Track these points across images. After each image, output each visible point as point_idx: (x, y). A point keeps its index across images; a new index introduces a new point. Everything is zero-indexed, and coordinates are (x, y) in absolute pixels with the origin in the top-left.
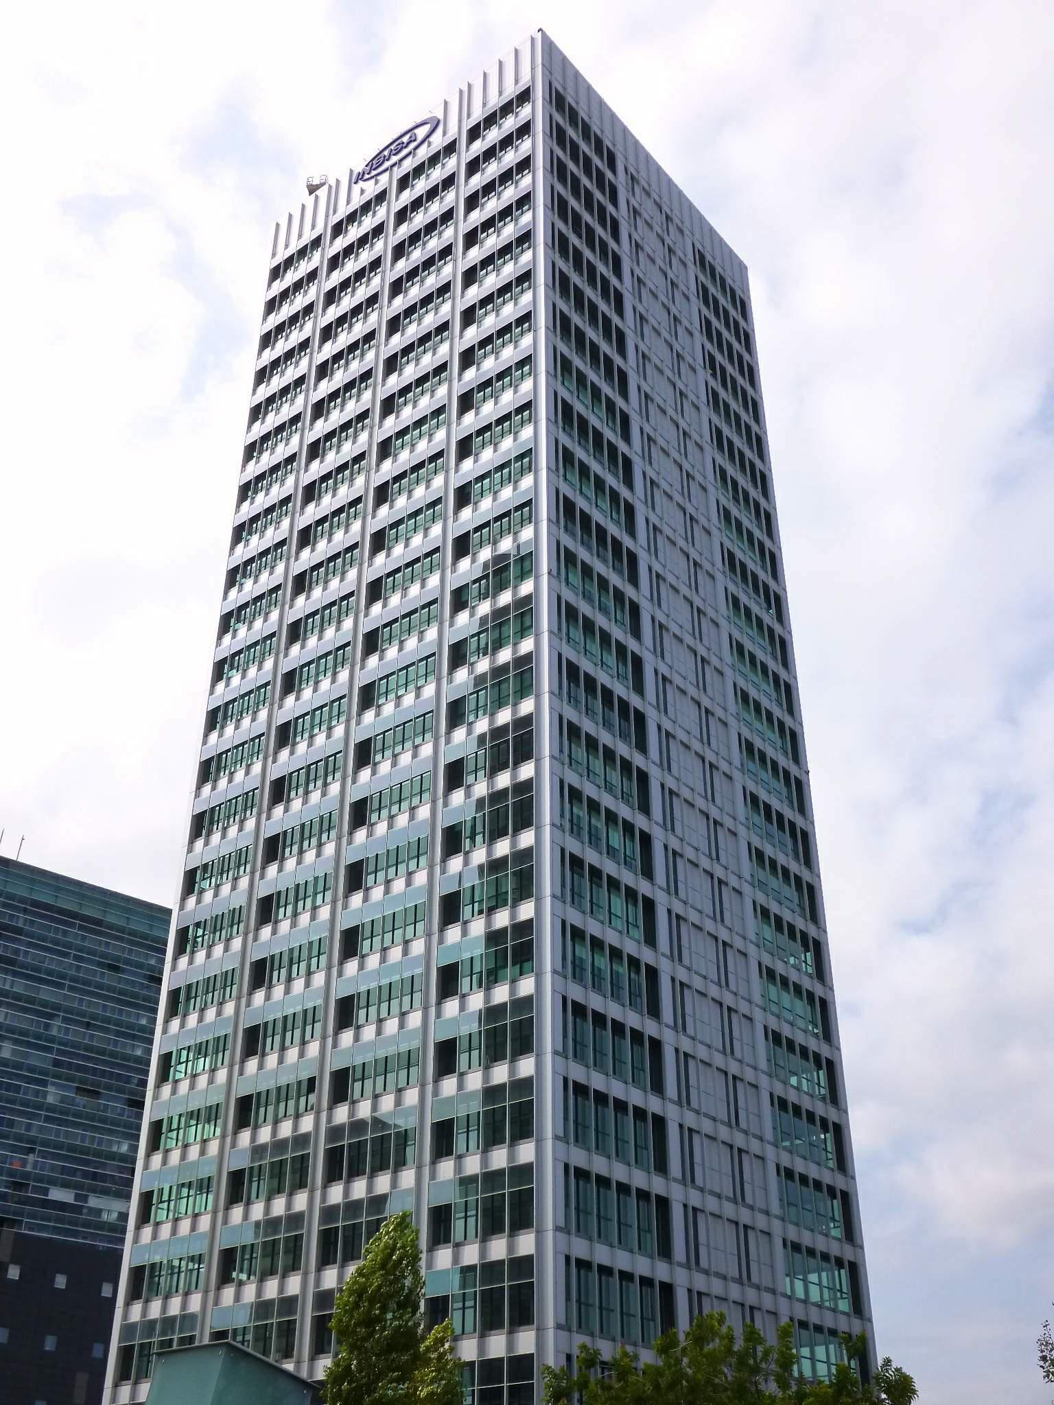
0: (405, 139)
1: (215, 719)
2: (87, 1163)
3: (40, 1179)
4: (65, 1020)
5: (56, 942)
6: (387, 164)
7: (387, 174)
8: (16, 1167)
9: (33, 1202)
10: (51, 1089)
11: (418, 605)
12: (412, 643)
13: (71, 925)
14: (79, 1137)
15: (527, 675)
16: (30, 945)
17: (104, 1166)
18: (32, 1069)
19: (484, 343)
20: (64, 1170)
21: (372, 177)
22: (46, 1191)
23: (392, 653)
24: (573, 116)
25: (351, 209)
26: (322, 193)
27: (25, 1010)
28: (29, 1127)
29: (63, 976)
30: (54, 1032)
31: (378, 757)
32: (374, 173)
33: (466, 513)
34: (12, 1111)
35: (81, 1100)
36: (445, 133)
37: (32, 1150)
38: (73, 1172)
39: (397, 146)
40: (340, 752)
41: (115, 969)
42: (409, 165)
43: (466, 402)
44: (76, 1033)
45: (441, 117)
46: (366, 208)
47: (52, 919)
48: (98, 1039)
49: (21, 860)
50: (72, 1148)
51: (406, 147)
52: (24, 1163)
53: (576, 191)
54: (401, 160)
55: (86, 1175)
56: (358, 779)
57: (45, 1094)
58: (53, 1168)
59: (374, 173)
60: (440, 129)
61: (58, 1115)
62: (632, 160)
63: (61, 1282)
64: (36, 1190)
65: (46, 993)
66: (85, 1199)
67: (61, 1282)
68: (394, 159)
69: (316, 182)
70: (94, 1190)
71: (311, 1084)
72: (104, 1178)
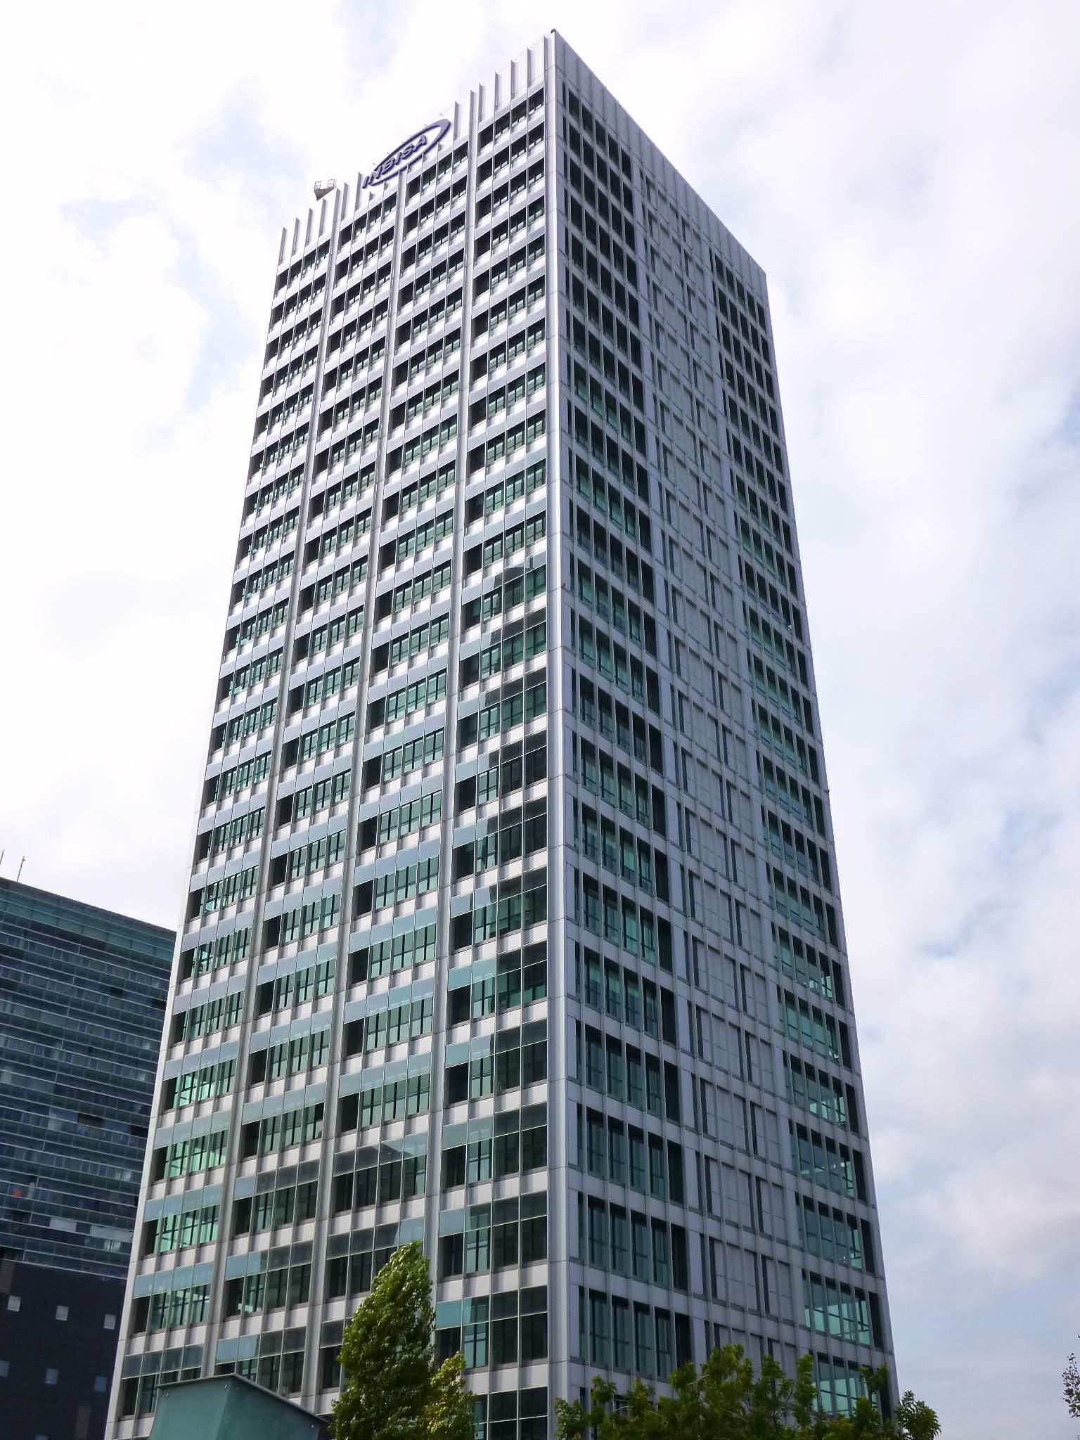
0: (415, 143)
1: (220, 737)
2: (89, 1192)
3: (40, 1208)
4: (67, 1045)
5: (58, 966)
6: (397, 168)
8: (17, 1196)
9: (34, 1232)
10: (52, 1116)
11: (428, 620)
13: (73, 948)
14: (81, 1165)
16: (31, 968)
17: (106, 1195)
18: (33, 1096)
19: (496, 352)
20: (65, 1199)
22: (47, 1221)
23: (402, 669)
24: (587, 119)
25: (359, 214)
26: (330, 198)
27: (26, 1035)
28: (29, 1155)
29: (65, 1001)
30: (56, 1058)
32: (383, 177)
33: (478, 526)
34: (12, 1139)
35: (83, 1127)
36: (455, 137)
37: (32, 1179)
38: (75, 1201)
39: (406, 149)
41: (118, 993)
42: (419, 169)
44: (78, 1059)
45: (452, 120)
46: (375, 213)
47: (54, 942)
48: (101, 1065)
50: (74, 1177)
51: (416, 151)
52: (24, 1192)
53: (590, 195)
54: (411, 164)
55: (88, 1204)
57: (46, 1121)
58: (54, 1197)
61: (60, 1143)
65: (47, 1018)
66: (87, 1229)
68: (404, 163)
69: (324, 186)
70: (96, 1220)
72: (106, 1207)
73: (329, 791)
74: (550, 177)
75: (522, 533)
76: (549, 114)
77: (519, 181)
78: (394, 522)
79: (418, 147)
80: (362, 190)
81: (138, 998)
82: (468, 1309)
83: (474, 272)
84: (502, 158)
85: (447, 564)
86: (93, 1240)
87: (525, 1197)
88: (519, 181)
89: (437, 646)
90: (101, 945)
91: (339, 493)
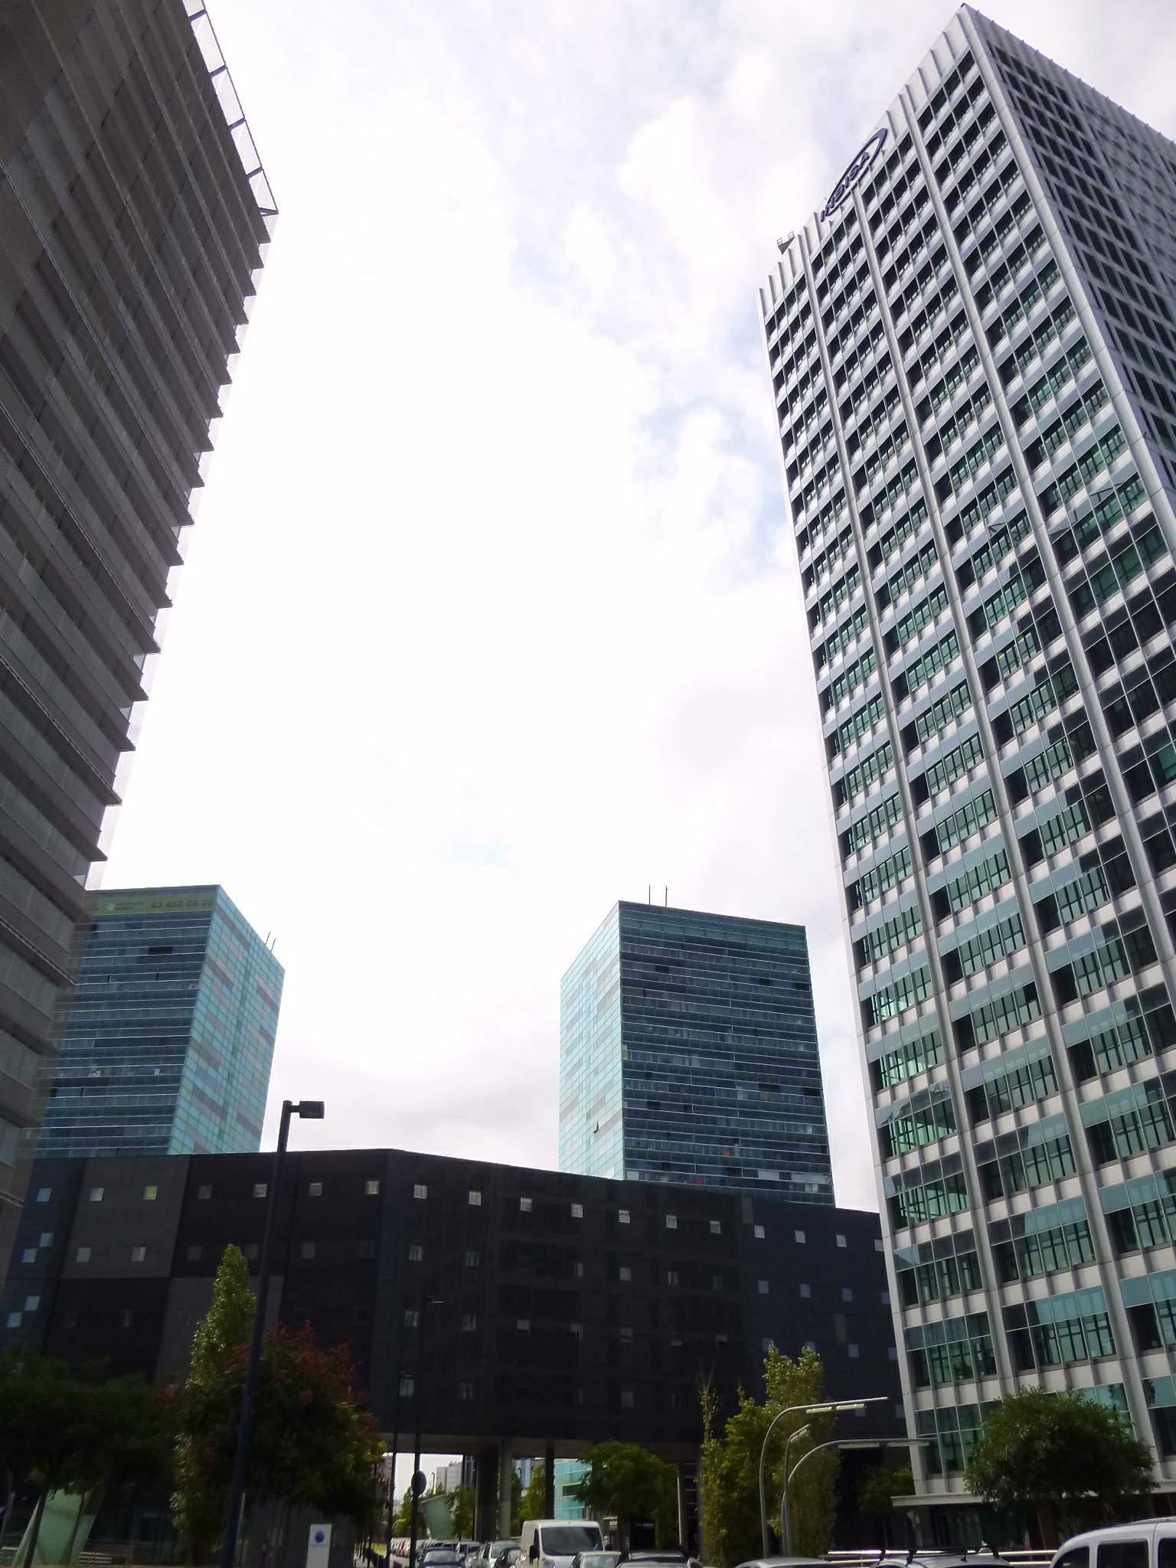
0: (859, 163)
1: (827, 699)
2: (783, 1146)
3: (748, 1163)
4: (736, 1030)
5: (712, 968)
6: (847, 191)
7: (851, 196)
8: (726, 1155)
9: (747, 1183)
10: (739, 1089)
11: (936, 641)
12: (940, 678)
13: (721, 952)
14: (771, 1125)
15: (1066, 675)
16: (693, 974)
17: (797, 1147)
18: (720, 1074)
19: (878, 499)
20: (765, 1154)
21: (838, 207)
22: (755, 1174)
23: (923, 692)
24: (1018, 66)
25: (825, 242)
26: (795, 246)
27: (702, 1027)
28: (728, 1122)
29: (726, 995)
30: (730, 1042)
31: (934, 790)
32: (837, 204)
33: (898, 656)
34: (712, 1111)
35: (765, 1095)
36: (895, 136)
37: (736, 1141)
38: (774, 1155)
39: (853, 171)
40: (897, 793)
41: (767, 982)
42: (869, 179)
43: (876, 556)
44: (747, 1040)
45: (887, 126)
46: (839, 234)
47: (706, 950)
48: (767, 1042)
49: (670, 905)
50: (768, 1136)
51: (861, 167)
52: (732, 1152)
53: (1043, 121)
54: (859, 180)
55: (784, 1156)
56: (991, 698)
57: (735, 1093)
58: (756, 1153)
59: (837, 204)
60: (890, 135)
61: (749, 1110)
62: (1081, 97)
63: (800, 1237)
64: (746, 1173)
65: (716, 1011)
66: (789, 1176)
67: (800, 1237)
68: (852, 183)
69: (786, 240)
70: (794, 1168)
71: (1031, 992)
72: (800, 1157)
73: (867, 828)
74: (945, 226)
75: (988, 555)
76: (986, 67)
77: (864, 346)
78: (881, 569)
79: (862, 164)
80: (820, 223)
81: (781, 984)
82: (1163, 1183)
83: (845, 436)
84: (845, 332)
85: (941, 588)
86: (795, 1184)
87: (960, 1407)
88: (864, 346)
89: (934, 676)
90: (744, 946)
91: (825, 562)
